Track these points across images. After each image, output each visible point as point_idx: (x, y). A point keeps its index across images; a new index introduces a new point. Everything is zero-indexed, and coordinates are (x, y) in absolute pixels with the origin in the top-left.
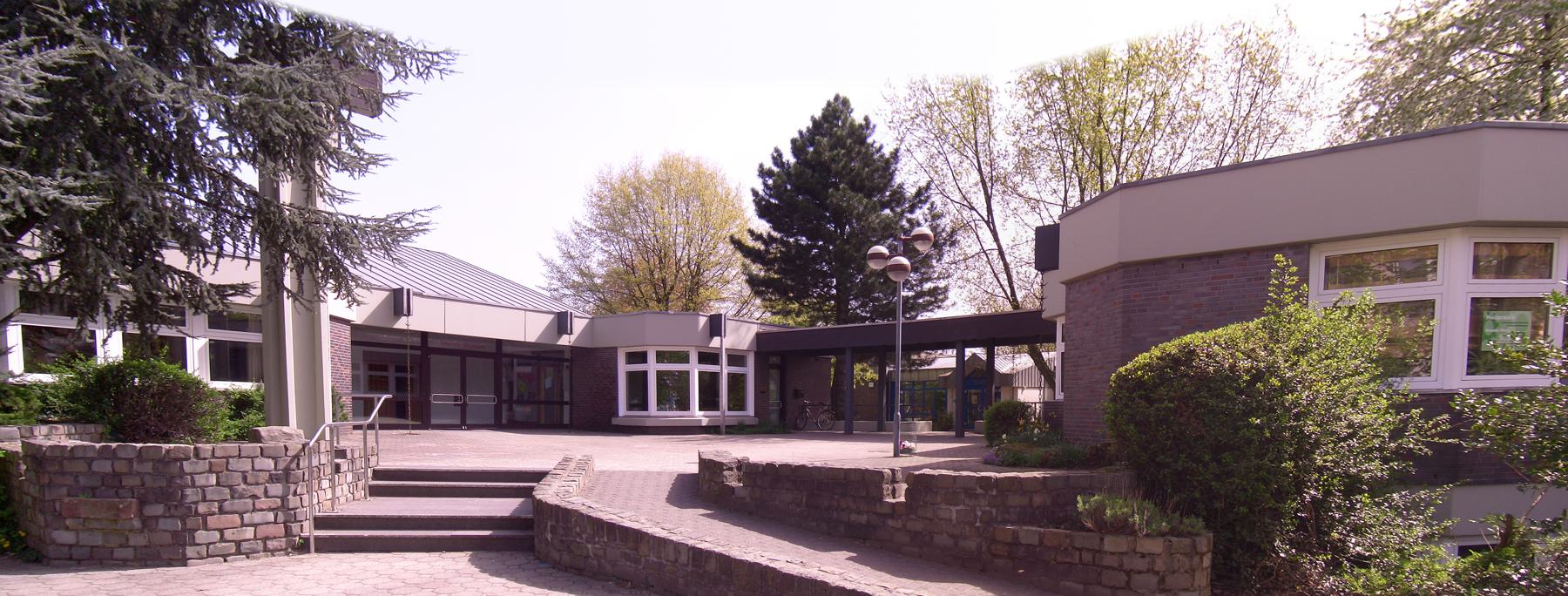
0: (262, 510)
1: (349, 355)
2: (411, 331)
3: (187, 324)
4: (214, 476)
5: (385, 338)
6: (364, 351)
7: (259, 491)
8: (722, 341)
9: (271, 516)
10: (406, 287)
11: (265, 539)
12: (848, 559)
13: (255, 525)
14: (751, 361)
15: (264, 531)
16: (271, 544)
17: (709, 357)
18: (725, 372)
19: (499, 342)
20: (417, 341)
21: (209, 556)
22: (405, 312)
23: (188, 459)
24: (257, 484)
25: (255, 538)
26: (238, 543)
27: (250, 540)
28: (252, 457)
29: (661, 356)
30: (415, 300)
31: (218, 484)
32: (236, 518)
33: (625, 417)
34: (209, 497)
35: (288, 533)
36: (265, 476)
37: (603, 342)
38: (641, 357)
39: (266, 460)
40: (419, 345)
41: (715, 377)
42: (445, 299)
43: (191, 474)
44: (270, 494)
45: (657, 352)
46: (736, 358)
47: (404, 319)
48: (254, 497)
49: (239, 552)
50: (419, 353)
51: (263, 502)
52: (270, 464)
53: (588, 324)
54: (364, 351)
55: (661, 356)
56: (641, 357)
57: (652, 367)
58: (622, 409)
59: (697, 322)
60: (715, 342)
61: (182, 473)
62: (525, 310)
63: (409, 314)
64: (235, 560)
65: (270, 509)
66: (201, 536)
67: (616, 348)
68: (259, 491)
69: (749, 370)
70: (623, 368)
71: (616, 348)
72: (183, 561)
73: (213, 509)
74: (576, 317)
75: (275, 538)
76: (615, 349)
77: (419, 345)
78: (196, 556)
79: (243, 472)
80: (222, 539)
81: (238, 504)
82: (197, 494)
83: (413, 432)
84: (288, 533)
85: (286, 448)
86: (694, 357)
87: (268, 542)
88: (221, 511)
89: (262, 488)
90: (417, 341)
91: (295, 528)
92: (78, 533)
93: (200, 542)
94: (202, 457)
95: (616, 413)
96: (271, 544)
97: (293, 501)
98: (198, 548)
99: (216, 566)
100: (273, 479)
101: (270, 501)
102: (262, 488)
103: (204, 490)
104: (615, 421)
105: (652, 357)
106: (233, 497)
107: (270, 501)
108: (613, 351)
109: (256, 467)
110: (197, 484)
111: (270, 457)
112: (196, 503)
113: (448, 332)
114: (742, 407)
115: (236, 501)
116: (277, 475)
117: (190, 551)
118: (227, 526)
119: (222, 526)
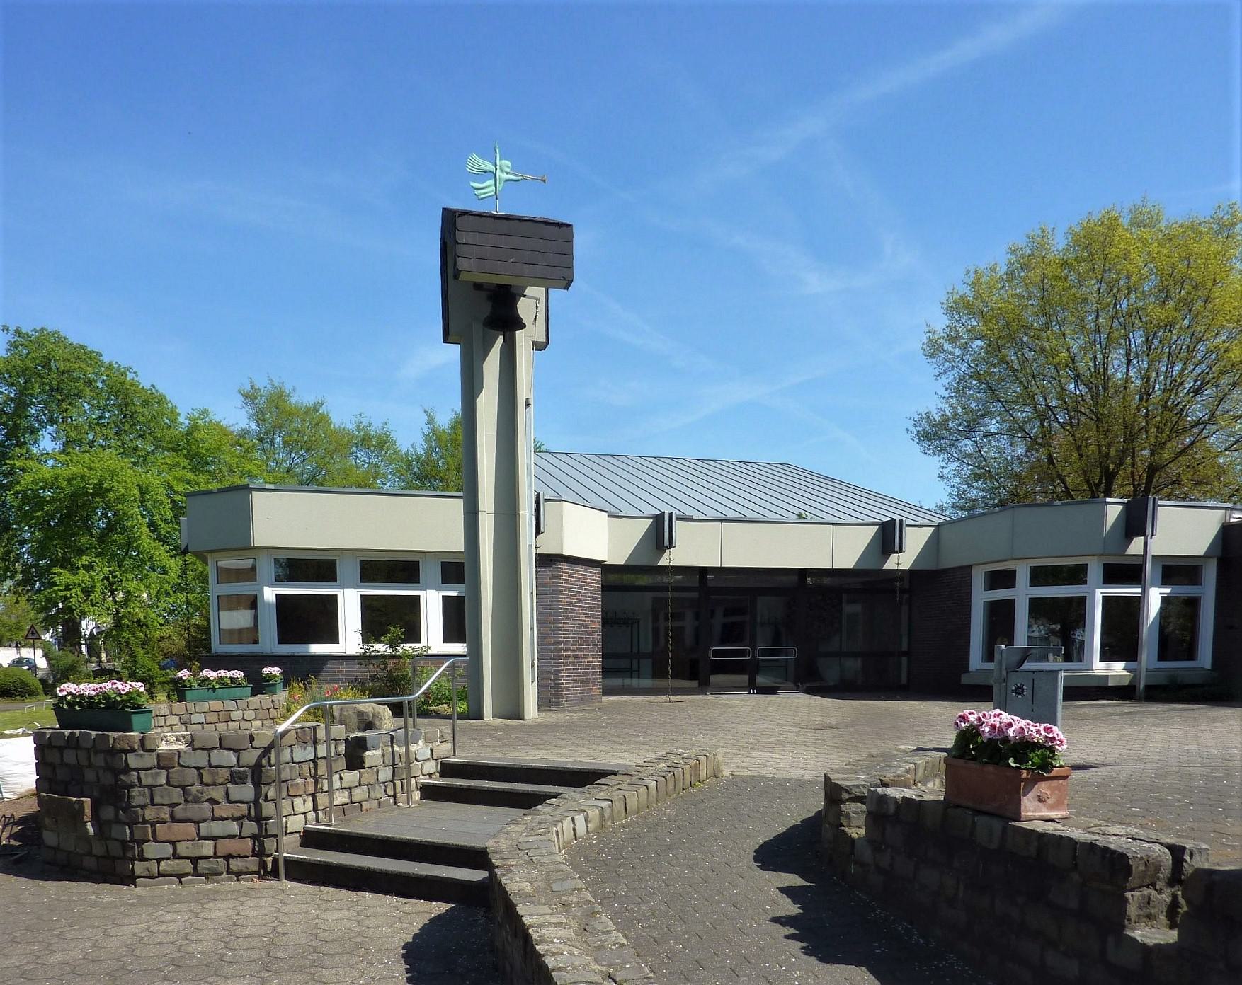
0: (223, 819)
1: (598, 603)
2: (673, 567)
3: (421, 581)
4: (164, 773)
5: (643, 580)
6: (444, 597)
7: (219, 793)
8: (1146, 544)
9: (234, 828)
10: (667, 510)
11: (228, 857)
12: (787, 937)
13: (215, 838)
14: (1210, 575)
15: (226, 846)
16: (236, 864)
17: (1130, 572)
18: (1100, 593)
19: (803, 573)
20: (695, 581)
21: (160, 875)
22: (897, 549)
23: (133, 751)
24: (215, 784)
25: (216, 856)
26: (194, 860)
27: (210, 857)
28: (208, 750)
29: (1040, 576)
30: (679, 527)
31: (168, 783)
32: (191, 827)
33: (978, 671)
34: (157, 800)
35: (260, 853)
36: (225, 774)
37: (950, 560)
38: (1002, 579)
39: (225, 752)
40: (697, 585)
41: (1134, 607)
42: (721, 521)
43: (137, 770)
44: (232, 798)
45: (361, 562)
46: (1174, 571)
47: (894, 556)
48: (213, 801)
49: (196, 872)
50: (696, 595)
51: (224, 809)
52: (231, 758)
53: (934, 530)
54: (444, 597)
55: (1040, 576)
56: (1002, 579)
57: (1023, 593)
58: (976, 659)
59: (1101, 517)
60: (1136, 546)
61: (127, 770)
62: (833, 524)
63: (901, 551)
64: (191, 882)
65: (233, 819)
66: (151, 849)
67: (970, 567)
68: (219, 793)
69: (1207, 592)
70: (981, 596)
71: (970, 567)
72: (129, 879)
73: (163, 816)
74: (907, 526)
75: (240, 856)
76: (969, 568)
77: (697, 585)
78: (146, 873)
79: (198, 769)
80: (176, 856)
81: (193, 810)
82: (144, 795)
83: (674, 698)
84: (260, 853)
85: (252, 738)
86: (1095, 571)
87: (231, 861)
88: (174, 819)
89: (221, 790)
90: (695, 581)
91: (270, 845)
92: (198, 834)
93: (150, 857)
94: (148, 748)
95: (966, 668)
96: (236, 864)
97: (268, 809)
98: (147, 864)
99: (167, 887)
100: (236, 778)
101: (232, 807)
102: (221, 790)
103: (152, 791)
104: (965, 679)
105: (1023, 577)
106: (186, 801)
107: (232, 807)
108: (965, 572)
109: (214, 763)
110: (144, 783)
111: (230, 749)
112: (143, 807)
113: (727, 563)
114: (1190, 652)
115: (190, 806)
116: (239, 772)
117: (139, 867)
118: (179, 839)
119: (173, 839)
